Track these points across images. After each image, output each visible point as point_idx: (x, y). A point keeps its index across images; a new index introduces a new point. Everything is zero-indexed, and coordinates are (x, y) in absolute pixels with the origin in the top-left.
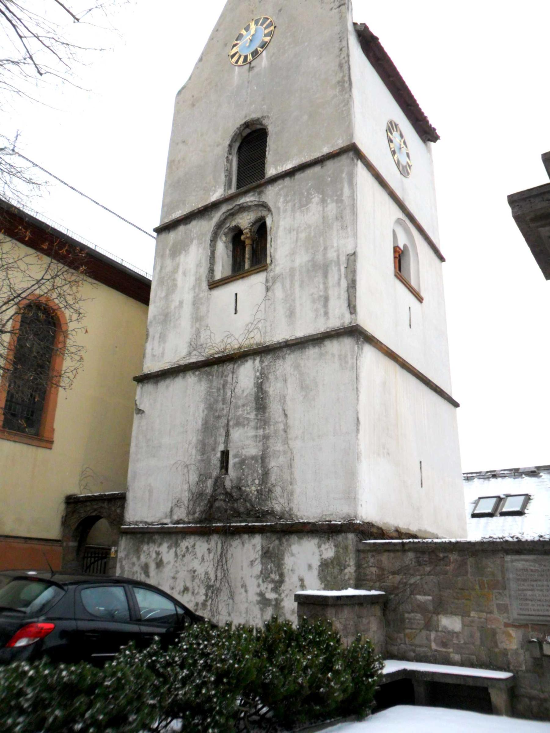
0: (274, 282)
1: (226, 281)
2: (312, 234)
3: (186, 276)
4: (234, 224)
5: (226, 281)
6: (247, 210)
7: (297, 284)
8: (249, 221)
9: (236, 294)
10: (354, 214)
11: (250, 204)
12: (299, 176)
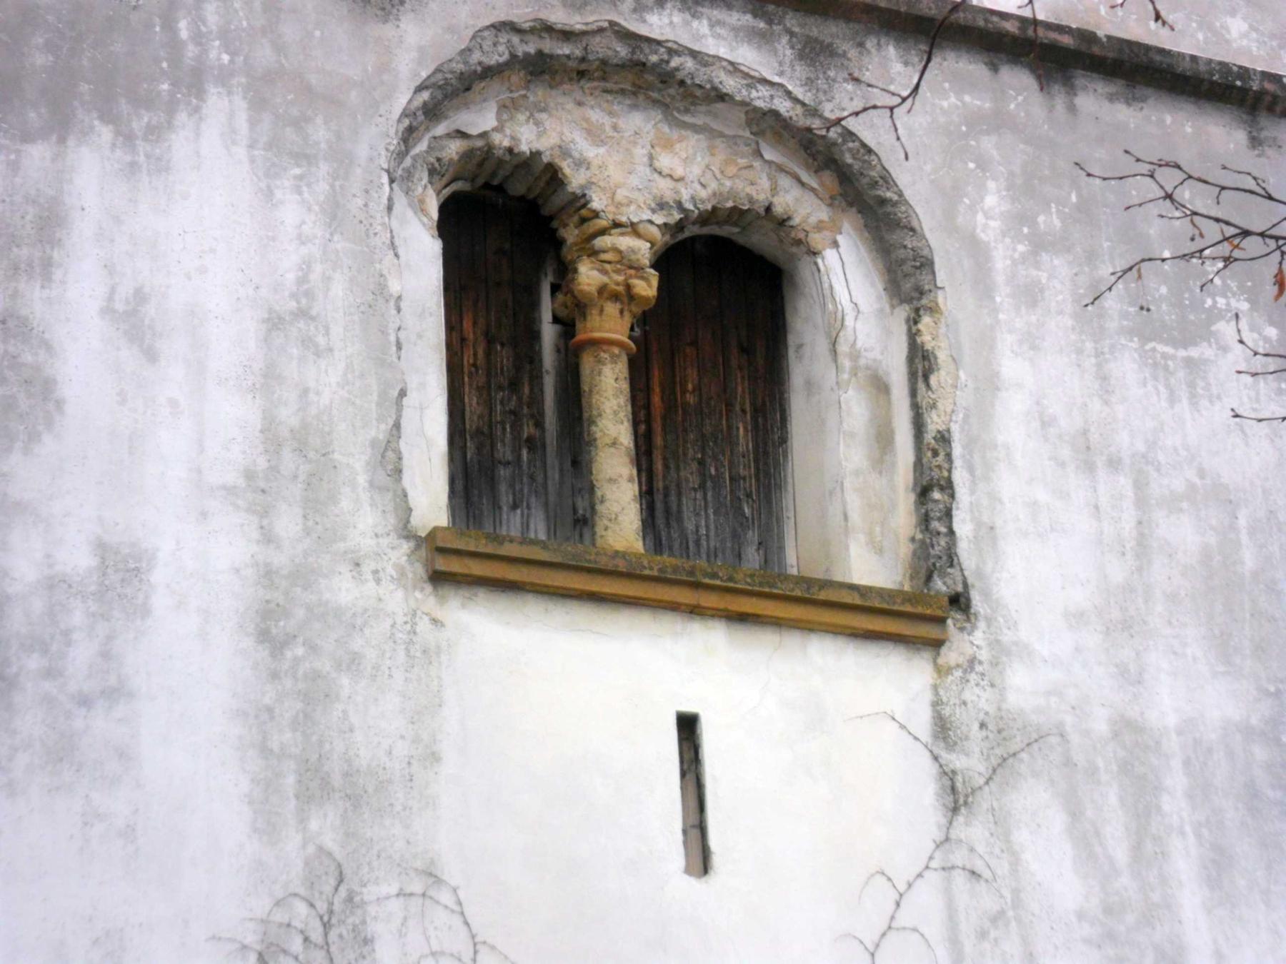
0: (1001, 766)
1: (512, 573)
2: (1249, 558)
3: (151, 356)
4: (527, 136)
5: (512, 573)
6: (665, 107)
7: (1184, 861)
8: (664, 187)
9: (688, 726)
10: (575, 463)
11: (730, 84)
12: (1095, 103)
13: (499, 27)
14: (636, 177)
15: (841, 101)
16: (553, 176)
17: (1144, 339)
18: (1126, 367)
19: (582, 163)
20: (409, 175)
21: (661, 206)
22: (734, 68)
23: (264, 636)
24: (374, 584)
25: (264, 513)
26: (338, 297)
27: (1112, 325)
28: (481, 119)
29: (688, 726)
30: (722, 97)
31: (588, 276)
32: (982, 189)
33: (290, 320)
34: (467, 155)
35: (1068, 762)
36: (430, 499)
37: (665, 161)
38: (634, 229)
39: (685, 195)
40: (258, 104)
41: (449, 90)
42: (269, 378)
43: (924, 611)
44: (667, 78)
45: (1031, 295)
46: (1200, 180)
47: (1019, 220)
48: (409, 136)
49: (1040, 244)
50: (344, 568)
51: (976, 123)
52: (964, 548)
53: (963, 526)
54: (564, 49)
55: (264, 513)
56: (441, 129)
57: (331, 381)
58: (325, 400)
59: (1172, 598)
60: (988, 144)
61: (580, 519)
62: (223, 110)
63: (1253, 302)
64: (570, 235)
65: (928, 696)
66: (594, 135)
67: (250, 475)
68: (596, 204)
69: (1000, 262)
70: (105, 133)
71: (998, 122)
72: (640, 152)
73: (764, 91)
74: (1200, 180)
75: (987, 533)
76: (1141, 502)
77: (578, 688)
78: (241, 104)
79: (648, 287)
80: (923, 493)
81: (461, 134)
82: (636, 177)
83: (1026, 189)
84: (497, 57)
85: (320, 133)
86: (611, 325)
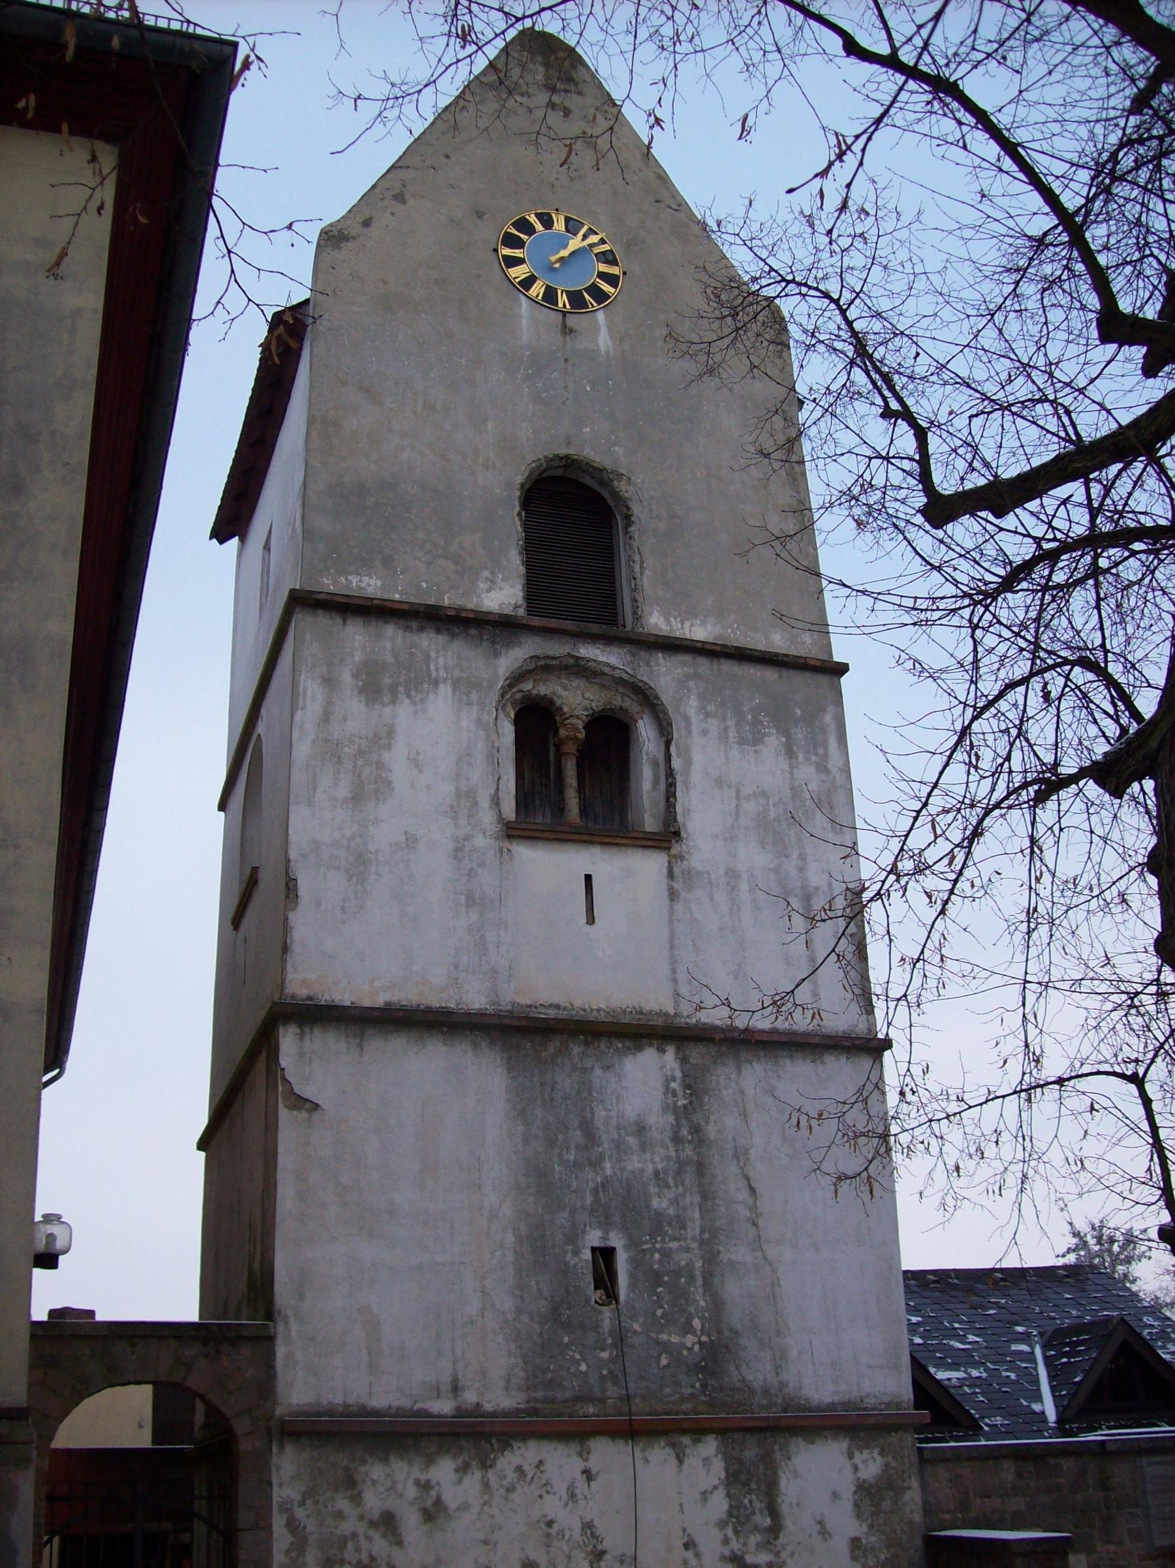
3: (421, 772)
4: (543, 690)
9: (588, 878)
11: (607, 670)
13: (531, 658)
14: (576, 701)
15: (643, 675)
16: (552, 702)
17: (741, 744)
18: (735, 753)
19: (560, 697)
20: (504, 705)
21: (586, 709)
22: (608, 665)
23: (455, 857)
24: (484, 841)
25: (456, 818)
26: (480, 748)
27: (731, 740)
28: (528, 686)
29: (588, 878)
30: (605, 674)
31: (563, 732)
32: (689, 697)
33: (466, 756)
34: (523, 697)
35: (710, 883)
36: (509, 809)
37: (587, 695)
38: (578, 717)
39: (594, 705)
40: (454, 690)
41: (516, 678)
42: (458, 777)
43: (667, 837)
44: (586, 669)
45: (704, 732)
46: (797, 986)
47: (702, 708)
48: (503, 695)
49: (707, 715)
50: (481, 835)
51: (688, 677)
52: (679, 818)
53: (679, 809)
54: (554, 662)
55: (456, 818)
56: (515, 690)
57: (477, 774)
58: (475, 781)
59: (747, 828)
60: (692, 684)
61: (560, 809)
62: (445, 690)
63: (778, 730)
64: (558, 718)
65: (666, 864)
66: (565, 688)
67: (451, 807)
68: (565, 710)
69: (694, 720)
70: (407, 701)
71: (695, 676)
72: (579, 692)
73: (618, 671)
74: (797, 986)
75: (687, 811)
76: (738, 798)
77: (552, 868)
78: (450, 690)
79: (581, 735)
80: (668, 800)
81: (521, 691)
82: (576, 701)
83: (704, 698)
84: (532, 666)
85: (474, 696)
86: (571, 748)
